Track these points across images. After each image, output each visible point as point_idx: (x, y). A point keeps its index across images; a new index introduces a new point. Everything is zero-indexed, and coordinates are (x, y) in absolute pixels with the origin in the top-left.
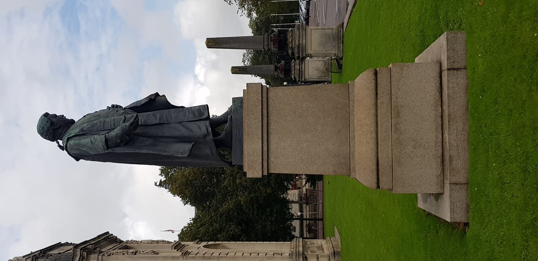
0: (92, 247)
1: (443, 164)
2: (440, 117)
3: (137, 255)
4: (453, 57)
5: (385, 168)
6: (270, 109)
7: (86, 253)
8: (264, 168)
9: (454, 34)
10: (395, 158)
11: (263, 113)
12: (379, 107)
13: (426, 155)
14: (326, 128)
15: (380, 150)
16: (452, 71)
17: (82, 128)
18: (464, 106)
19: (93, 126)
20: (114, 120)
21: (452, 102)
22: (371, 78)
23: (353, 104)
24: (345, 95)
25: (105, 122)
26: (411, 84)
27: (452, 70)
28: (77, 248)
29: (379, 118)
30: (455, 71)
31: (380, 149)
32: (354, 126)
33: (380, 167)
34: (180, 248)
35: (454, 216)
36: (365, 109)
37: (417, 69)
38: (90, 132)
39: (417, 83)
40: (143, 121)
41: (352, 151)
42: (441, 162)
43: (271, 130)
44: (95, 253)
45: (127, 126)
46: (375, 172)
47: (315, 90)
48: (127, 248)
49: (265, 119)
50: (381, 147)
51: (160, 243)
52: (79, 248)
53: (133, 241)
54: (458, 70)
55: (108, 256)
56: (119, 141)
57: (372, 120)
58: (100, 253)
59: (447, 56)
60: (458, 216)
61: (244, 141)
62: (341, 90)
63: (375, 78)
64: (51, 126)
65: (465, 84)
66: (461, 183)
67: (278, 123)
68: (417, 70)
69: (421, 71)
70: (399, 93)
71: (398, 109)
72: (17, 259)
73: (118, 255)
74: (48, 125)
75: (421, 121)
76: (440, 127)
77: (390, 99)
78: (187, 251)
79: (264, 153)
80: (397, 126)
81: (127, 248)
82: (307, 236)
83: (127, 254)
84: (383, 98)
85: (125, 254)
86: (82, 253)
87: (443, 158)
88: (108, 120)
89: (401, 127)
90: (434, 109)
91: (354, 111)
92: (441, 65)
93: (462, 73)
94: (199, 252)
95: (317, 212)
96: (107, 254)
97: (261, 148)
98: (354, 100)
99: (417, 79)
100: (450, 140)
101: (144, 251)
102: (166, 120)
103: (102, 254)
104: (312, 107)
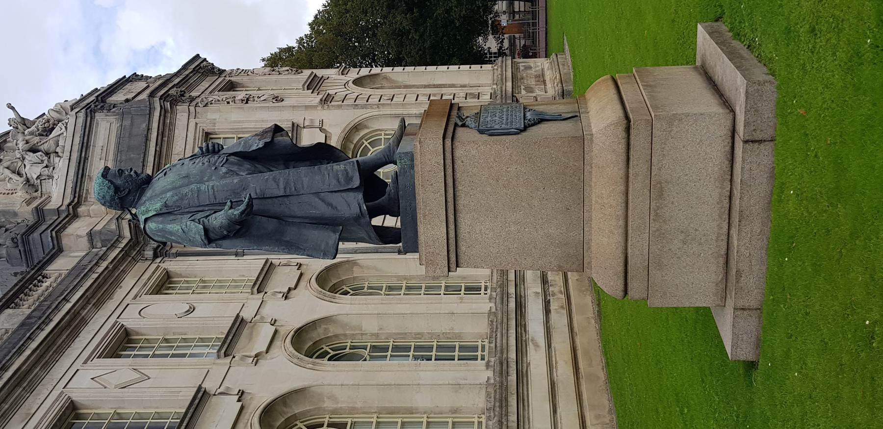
0: (177, 93)
1: (727, 266)
2: (728, 198)
3: (250, 104)
4: (754, 122)
5: (638, 270)
6: (458, 175)
7: (168, 103)
8: (451, 262)
9: (759, 85)
10: (653, 258)
12: (630, 179)
13: (701, 254)
14: (547, 204)
15: (630, 244)
16: (751, 145)
17: (165, 202)
18: (765, 199)
19: (182, 199)
20: (213, 187)
21: (748, 191)
22: (620, 136)
23: (590, 170)
24: (578, 154)
25: (199, 191)
26: (684, 147)
27: (751, 143)
28: (154, 97)
30: (756, 145)
31: (630, 243)
32: (591, 202)
33: (629, 268)
34: (315, 87)
35: (736, 352)
36: (608, 182)
37: (694, 125)
38: (178, 209)
39: (693, 146)
40: (259, 191)
41: (587, 239)
42: (724, 264)
43: (460, 207)
44: (183, 102)
45: (235, 215)
46: (622, 275)
47: (529, 147)
48: (231, 86)
51: (284, 73)
52: (156, 97)
53: (239, 71)
54: (760, 143)
55: (204, 106)
56: (225, 233)
57: (621, 199)
58: (191, 101)
59: (745, 120)
60: (742, 352)
61: (418, 221)
62: (570, 146)
63: (626, 136)
65: (769, 165)
66: (751, 308)
67: (471, 195)
68: (695, 126)
69: (702, 126)
71: (661, 186)
72: (61, 107)
73: (220, 104)
74: (111, 192)
75: (696, 204)
76: (726, 212)
78: (329, 94)
79: (450, 241)
80: (658, 211)
81: (231, 86)
82: (519, 3)
83: (235, 103)
84: (638, 166)
85: (231, 102)
86: (162, 104)
87: (727, 258)
88: (203, 187)
90: (720, 186)
91: (591, 180)
92: (735, 118)
93: (768, 147)
94: (347, 95)
95: (537, 21)
96: (203, 103)
97: (446, 235)
98: (592, 164)
100: (740, 247)
101: (260, 97)
102: (294, 189)
103: (194, 103)
104: (525, 173)
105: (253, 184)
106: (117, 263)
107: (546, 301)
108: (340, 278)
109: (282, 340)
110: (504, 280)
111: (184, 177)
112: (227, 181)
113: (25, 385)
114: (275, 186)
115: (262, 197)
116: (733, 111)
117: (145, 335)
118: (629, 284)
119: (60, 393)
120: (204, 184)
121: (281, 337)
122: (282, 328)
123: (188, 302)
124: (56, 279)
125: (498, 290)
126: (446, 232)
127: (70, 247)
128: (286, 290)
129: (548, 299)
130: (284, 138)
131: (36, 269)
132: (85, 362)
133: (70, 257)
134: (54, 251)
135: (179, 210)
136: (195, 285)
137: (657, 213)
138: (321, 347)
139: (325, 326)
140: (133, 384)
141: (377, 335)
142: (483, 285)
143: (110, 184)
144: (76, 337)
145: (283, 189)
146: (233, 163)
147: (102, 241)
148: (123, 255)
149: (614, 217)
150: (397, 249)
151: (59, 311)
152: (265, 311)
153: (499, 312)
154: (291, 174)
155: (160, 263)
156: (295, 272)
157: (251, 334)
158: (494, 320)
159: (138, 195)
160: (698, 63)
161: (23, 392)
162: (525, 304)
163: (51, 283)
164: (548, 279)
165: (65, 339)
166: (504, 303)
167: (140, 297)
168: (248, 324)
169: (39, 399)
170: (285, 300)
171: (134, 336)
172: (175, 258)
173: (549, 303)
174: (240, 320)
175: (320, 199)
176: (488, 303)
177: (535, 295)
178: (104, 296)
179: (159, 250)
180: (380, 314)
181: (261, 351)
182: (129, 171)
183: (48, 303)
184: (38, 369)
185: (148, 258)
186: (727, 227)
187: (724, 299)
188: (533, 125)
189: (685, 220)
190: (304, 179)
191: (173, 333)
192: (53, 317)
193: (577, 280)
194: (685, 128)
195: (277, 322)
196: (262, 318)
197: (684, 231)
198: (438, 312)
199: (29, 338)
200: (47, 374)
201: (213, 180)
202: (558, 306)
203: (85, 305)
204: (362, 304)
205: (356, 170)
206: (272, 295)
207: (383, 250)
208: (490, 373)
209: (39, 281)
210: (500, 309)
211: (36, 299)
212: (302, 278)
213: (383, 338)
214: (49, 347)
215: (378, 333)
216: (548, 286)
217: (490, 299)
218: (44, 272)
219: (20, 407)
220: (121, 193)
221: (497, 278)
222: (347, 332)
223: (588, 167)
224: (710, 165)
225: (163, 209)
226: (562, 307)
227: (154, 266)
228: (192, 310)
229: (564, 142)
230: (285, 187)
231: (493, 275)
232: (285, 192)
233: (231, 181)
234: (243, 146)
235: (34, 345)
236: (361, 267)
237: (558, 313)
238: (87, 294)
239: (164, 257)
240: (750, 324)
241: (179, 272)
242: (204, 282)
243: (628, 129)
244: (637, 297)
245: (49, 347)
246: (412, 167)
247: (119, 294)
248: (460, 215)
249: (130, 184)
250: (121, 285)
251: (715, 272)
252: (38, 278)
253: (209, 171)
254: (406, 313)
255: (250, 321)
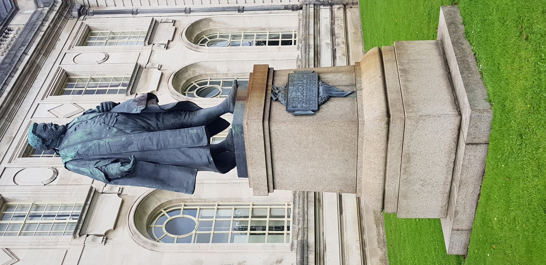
6: (273, 140)
8: (270, 187)
11: (266, 145)
16: (471, 146)
19: (88, 150)
21: (466, 171)
25: (99, 145)
29: (388, 168)
30: (474, 146)
31: (387, 184)
37: (434, 123)
38: (86, 157)
40: (140, 146)
49: (268, 150)
50: (388, 183)
54: (477, 145)
57: (382, 161)
63: (387, 126)
64: (43, 144)
70: (411, 143)
71: (409, 156)
74: (40, 143)
76: (451, 170)
77: (402, 145)
79: (269, 177)
88: (102, 143)
89: (411, 170)
97: (266, 175)
99: (433, 131)
105: (136, 141)
106: (55, 22)
107: (334, 49)
108: (201, 30)
109: (166, 82)
110: (307, 34)
111: (88, 134)
112: (117, 139)
113: (6, 117)
114: (150, 143)
115: (143, 150)
116: (460, 114)
117: (78, 76)
118: (385, 205)
119: (30, 122)
120: (102, 140)
121: (166, 79)
122: (166, 71)
123: (104, 51)
124: (17, 31)
125: (303, 42)
126: (266, 173)
127: (24, 7)
128: (166, 42)
129: (335, 48)
130: (154, 105)
131: (3, 24)
132: (43, 99)
133: (24, 14)
134: (13, 10)
135: (87, 157)
136: (107, 36)
137: (406, 170)
138: (191, 83)
139: (193, 69)
140: (73, 116)
141: (227, 74)
142: (293, 34)
143: (38, 138)
144: (35, 80)
145: (156, 146)
146: (121, 123)
147: (44, 3)
148: (58, 16)
149: (377, 170)
150: (237, 9)
151: (21, 62)
152: (154, 58)
153: (304, 60)
154: (161, 135)
155: (83, 20)
156: (171, 28)
157: (146, 76)
158: (300, 65)
159: (58, 142)
160: (439, 38)
161: (6, 122)
162: (320, 52)
163: (14, 35)
164: (335, 32)
165: (28, 82)
166: (307, 52)
167: (73, 48)
168: (144, 69)
169: (17, 126)
170: (166, 49)
171: (72, 76)
172: (92, 16)
173: (336, 51)
174: (138, 67)
175: (181, 152)
176: (296, 51)
177: (326, 45)
178: (50, 47)
179: (81, 11)
180: (228, 61)
181: (152, 91)
182: (50, 126)
183: (14, 52)
184: (13, 105)
185: (75, 17)
186: (451, 178)
187: (446, 215)
188: (324, 103)
189: (424, 174)
190: (170, 138)
191: (97, 74)
192: (19, 67)
193: (354, 32)
194: (427, 124)
195: (162, 67)
196: (153, 64)
197: (423, 180)
198: (265, 59)
199: (5, 84)
200: (19, 108)
201: (108, 138)
202: (341, 54)
203: (38, 56)
204: (216, 53)
205: (204, 134)
206: (158, 46)
207: (228, 10)
208: (299, 53)
209: (7, 34)
210: (304, 57)
211: (6, 48)
212: (177, 31)
213: (230, 76)
214: (18, 89)
215: (227, 73)
216: (335, 38)
217: (298, 48)
218: (9, 26)
219: (5, 133)
220: (46, 142)
221: (303, 33)
222: (207, 73)
223: (361, 139)
224: (443, 145)
225: (76, 157)
226: (344, 55)
227: (79, 23)
228: (107, 58)
229: (344, 124)
230: (157, 144)
231: (300, 29)
232: (158, 147)
233: (121, 139)
234: (127, 109)
235: (8, 89)
236: (215, 22)
237: (341, 59)
238: (38, 48)
239: (85, 15)
240: (462, 238)
241: (96, 27)
242: (113, 33)
243: (388, 123)
244: (390, 211)
245: (18, 89)
246: (242, 132)
247: (59, 45)
248: (276, 162)
249: (52, 136)
250: (59, 38)
251: (442, 201)
252: (5, 31)
253: (105, 130)
254: (244, 60)
255: (145, 67)
